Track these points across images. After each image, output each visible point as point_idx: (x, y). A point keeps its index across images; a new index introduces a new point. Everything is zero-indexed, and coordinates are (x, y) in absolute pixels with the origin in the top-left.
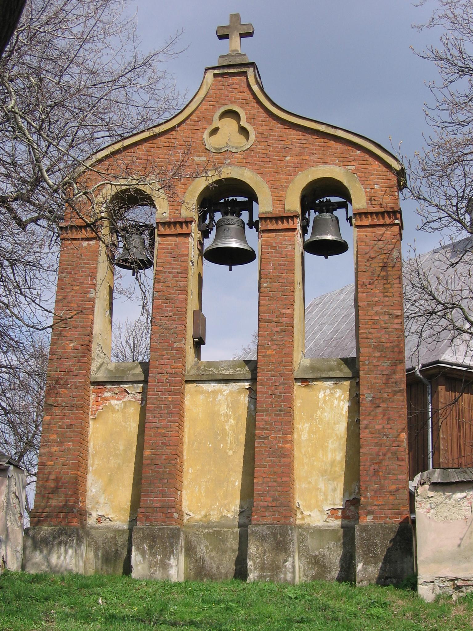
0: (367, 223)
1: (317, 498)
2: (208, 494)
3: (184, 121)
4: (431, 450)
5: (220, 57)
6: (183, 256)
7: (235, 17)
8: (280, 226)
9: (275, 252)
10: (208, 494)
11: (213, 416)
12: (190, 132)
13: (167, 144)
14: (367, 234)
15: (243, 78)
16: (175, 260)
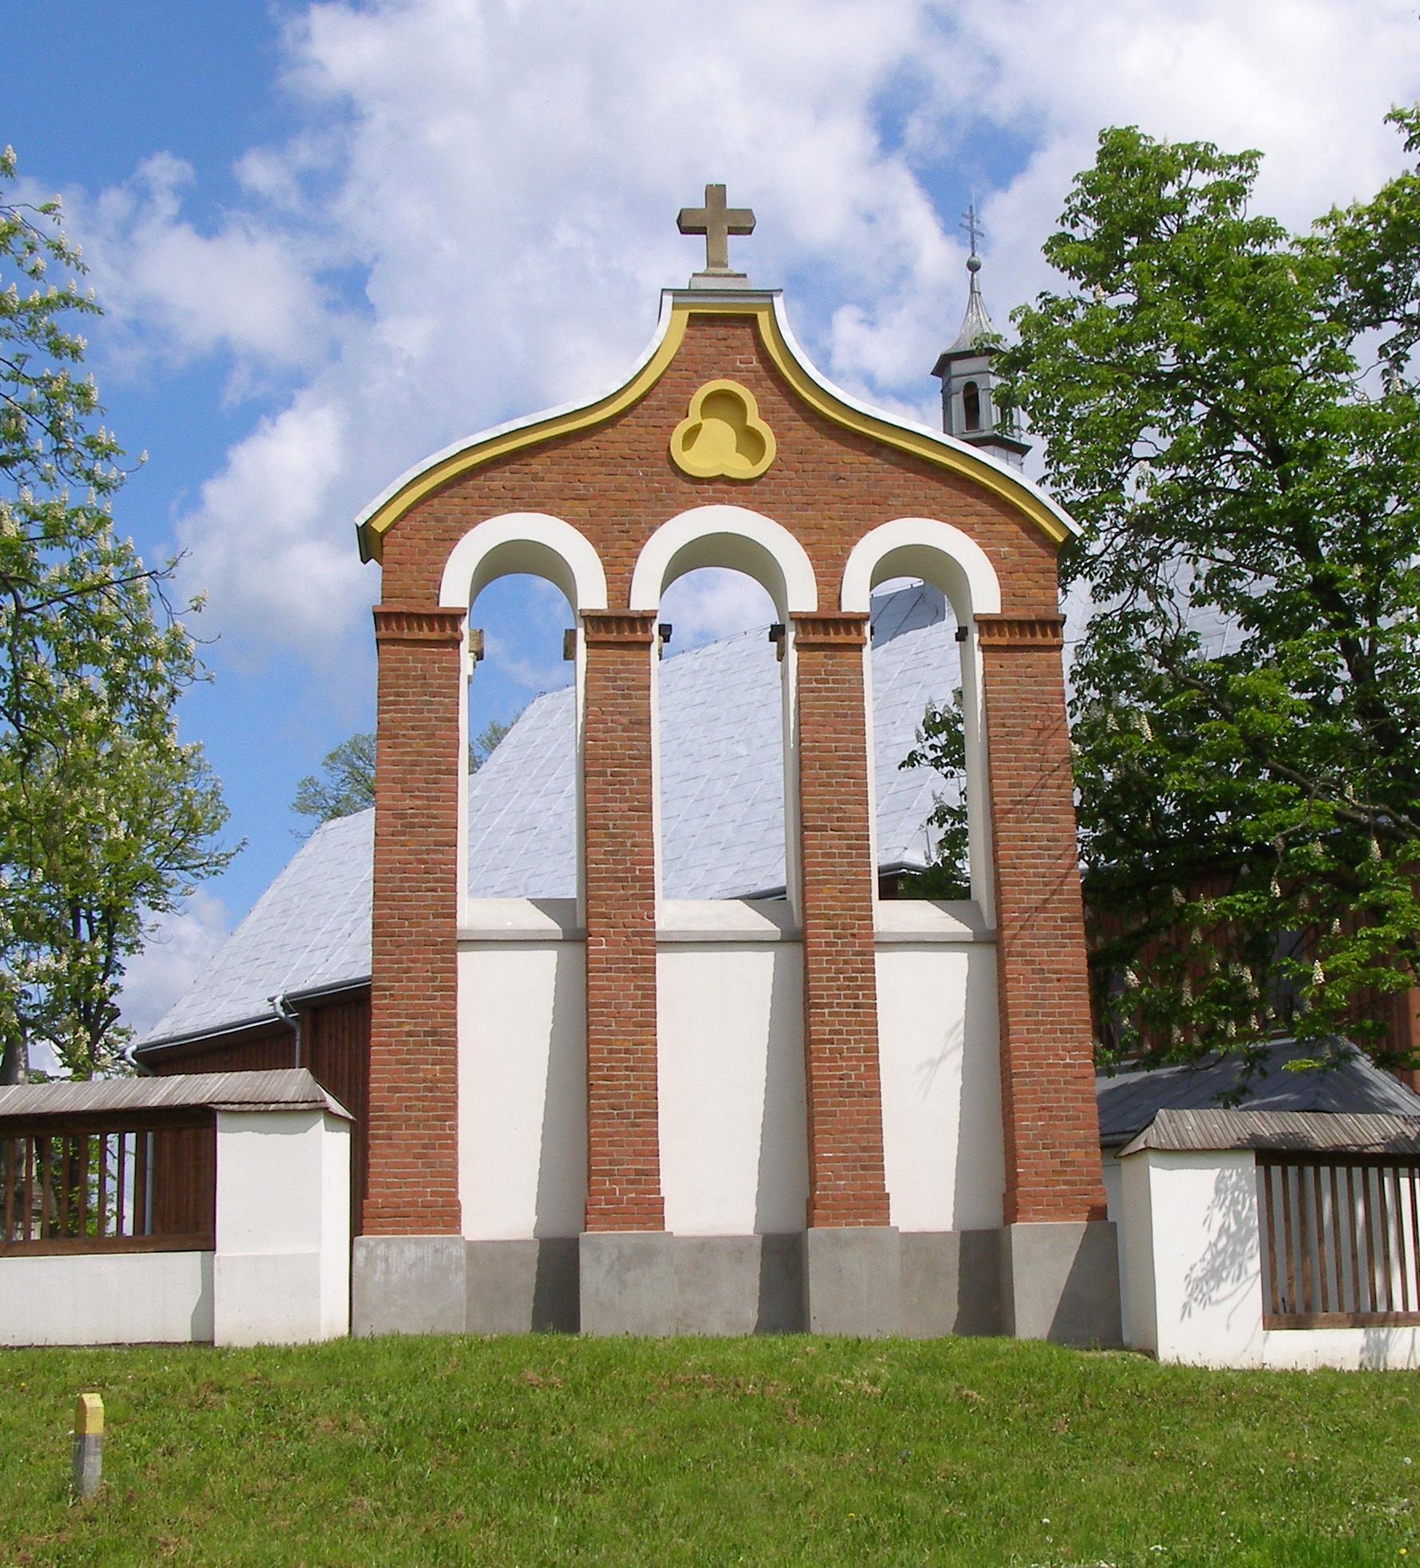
0: (1003, 641)
1: (925, 1174)
2: (713, 1171)
3: (633, 406)
4: (980, 696)
5: (749, 231)
6: (638, 688)
7: (716, 194)
8: (833, 638)
9: (826, 689)
10: (713, 1171)
11: (715, 1031)
12: (641, 430)
13: (595, 453)
14: (1004, 663)
15: (746, 333)
16: (624, 697)
